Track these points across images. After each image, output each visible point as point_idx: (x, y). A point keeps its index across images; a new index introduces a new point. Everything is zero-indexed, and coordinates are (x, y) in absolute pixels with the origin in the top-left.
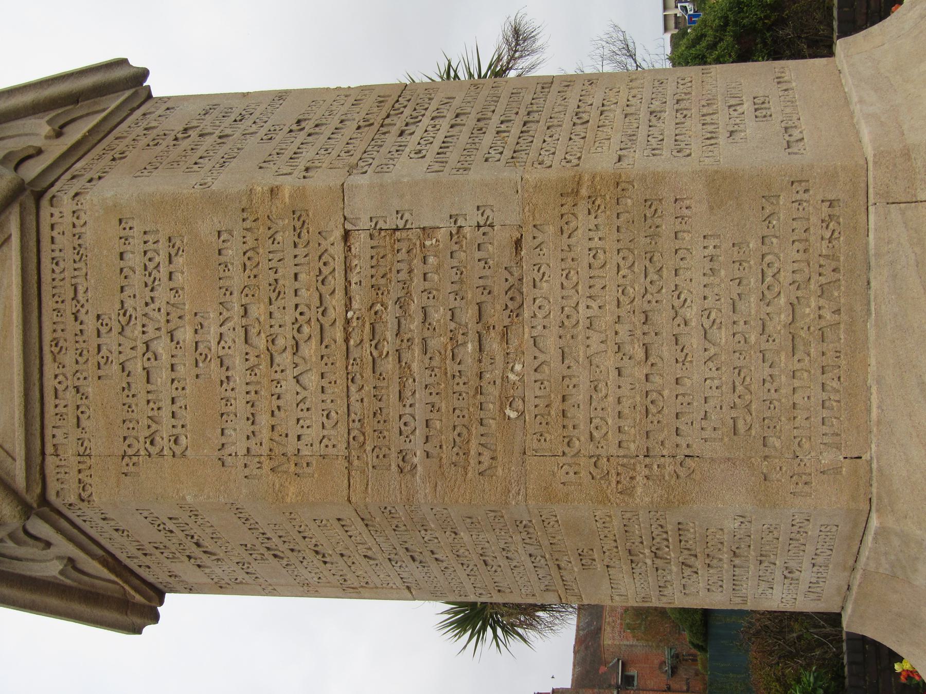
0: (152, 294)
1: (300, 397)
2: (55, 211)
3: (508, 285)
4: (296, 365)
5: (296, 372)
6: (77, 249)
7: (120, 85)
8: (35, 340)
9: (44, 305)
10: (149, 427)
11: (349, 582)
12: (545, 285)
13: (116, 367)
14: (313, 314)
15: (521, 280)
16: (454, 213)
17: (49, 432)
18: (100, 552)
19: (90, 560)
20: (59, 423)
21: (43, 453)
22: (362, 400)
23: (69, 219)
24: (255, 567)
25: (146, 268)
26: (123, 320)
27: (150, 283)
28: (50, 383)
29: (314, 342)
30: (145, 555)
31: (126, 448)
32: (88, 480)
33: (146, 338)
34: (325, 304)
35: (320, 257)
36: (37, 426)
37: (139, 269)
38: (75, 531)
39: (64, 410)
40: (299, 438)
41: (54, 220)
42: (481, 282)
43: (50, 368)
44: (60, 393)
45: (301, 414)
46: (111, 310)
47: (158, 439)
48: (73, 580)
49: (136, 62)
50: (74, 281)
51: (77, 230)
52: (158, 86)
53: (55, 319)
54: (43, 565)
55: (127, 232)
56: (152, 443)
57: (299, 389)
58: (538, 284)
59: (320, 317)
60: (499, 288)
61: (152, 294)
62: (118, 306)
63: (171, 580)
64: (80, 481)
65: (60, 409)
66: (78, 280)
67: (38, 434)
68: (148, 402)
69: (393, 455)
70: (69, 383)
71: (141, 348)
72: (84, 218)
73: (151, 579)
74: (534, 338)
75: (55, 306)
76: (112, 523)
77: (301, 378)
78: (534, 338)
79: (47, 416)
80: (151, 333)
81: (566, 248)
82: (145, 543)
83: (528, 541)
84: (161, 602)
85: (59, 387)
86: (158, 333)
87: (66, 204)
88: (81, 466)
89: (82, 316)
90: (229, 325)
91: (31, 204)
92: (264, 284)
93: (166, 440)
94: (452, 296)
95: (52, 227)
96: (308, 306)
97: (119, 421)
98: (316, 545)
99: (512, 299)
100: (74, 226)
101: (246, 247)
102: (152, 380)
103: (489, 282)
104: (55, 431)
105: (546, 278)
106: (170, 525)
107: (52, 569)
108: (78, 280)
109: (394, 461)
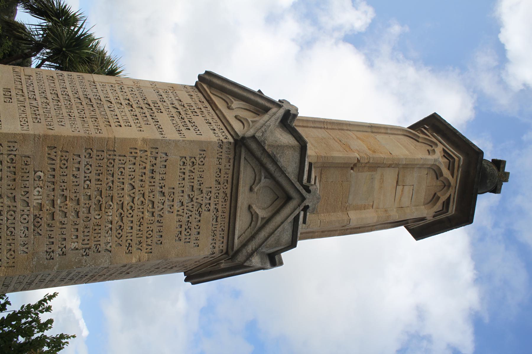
0: (188, 219)
1: (133, 180)
2: (221, 248)
3: (40, 228)
4: (134, 193)
5: (134, 190)
6: (215, 235)
7: (195, 276)
8: (233, 202)
9: (228, 214)
10: (194, 169)
11: (119, 87)
12: (23, 229)
13: (204, 191)
14: (125, 214)
15: (34, 230)
16: (64, 256)
17: (231, 167)
18: (217, 112)
19: (221, 109)
20: (227, 170)
21: (234, 158)
22: (107, 179)
23: (217, 246)
24: (157, 98)
25: (190, 229)
26: (200, 209)
27: (189, 224)
28: (229, 186)
29: (126, 203)
30: (201, 109)
31: (204, 161)
32: (219, 149)
33: (192, 203)
34: (99, 205)
35: (122, 236)
36: (235, 170)
37: (193, 229)
38: (226, 125)
39: (225, 175)
40: (134, 164)
41: (222, 245)
42: (52, 229)
43: (228, 191)
44: (226, 181)
45: (133, 173)
46: (205, 214)
47: (191, 164)
48: (228, 98)
49: (189, 284)
50: (217, 223)
51: (215, 241)
52: (182, 276)
53: (225, 209)
54: (239, 106)
55: (195, 242)
56: (193, 163)
57: (133, 184)
58: (26, 229)
59: (123, 213)
60: (44, 227)
61: (188, 219)
62: (202, 215)
63: (192, 93)
64: (222, 148)
65: (226, 176)
66: (215, 223)
67: (235, 167)
68: (193, 179)
69: (94, 157)
70: (222, 185)
71: (194, 199)
72: (211, 247)
73: (200, 95)
74: (28, 206)
75: (224, 214)
76: (211, 127)
77: (132, 188)
78: (28, 206)
79: (231, 173)
80: (190, 205)
81: (12, 244)
82: (200, 116)
83: (36, 109)
84: (197, 82)
85: (226, 184)
86: (188, 205)
87: (217, 250)
88: (221, 154)
89: (215, 211)
90: (159, 209)
91: (230, 250)
92: (145, 225)
93: (188, 164)
94: (66, 223)
95: (223, 242)
96: (127, 217)
97: (205, 171)
98: (132, 110)
99: (39, 222)
100: (215, 243)
101: (151, 239)
102: (191, 187)
103: (49, 229)
104: (229, 168)
105: (22, 232)
106: (190, 125)
107: (236, 104)
108: (215, 223)
109: (94, 154)
